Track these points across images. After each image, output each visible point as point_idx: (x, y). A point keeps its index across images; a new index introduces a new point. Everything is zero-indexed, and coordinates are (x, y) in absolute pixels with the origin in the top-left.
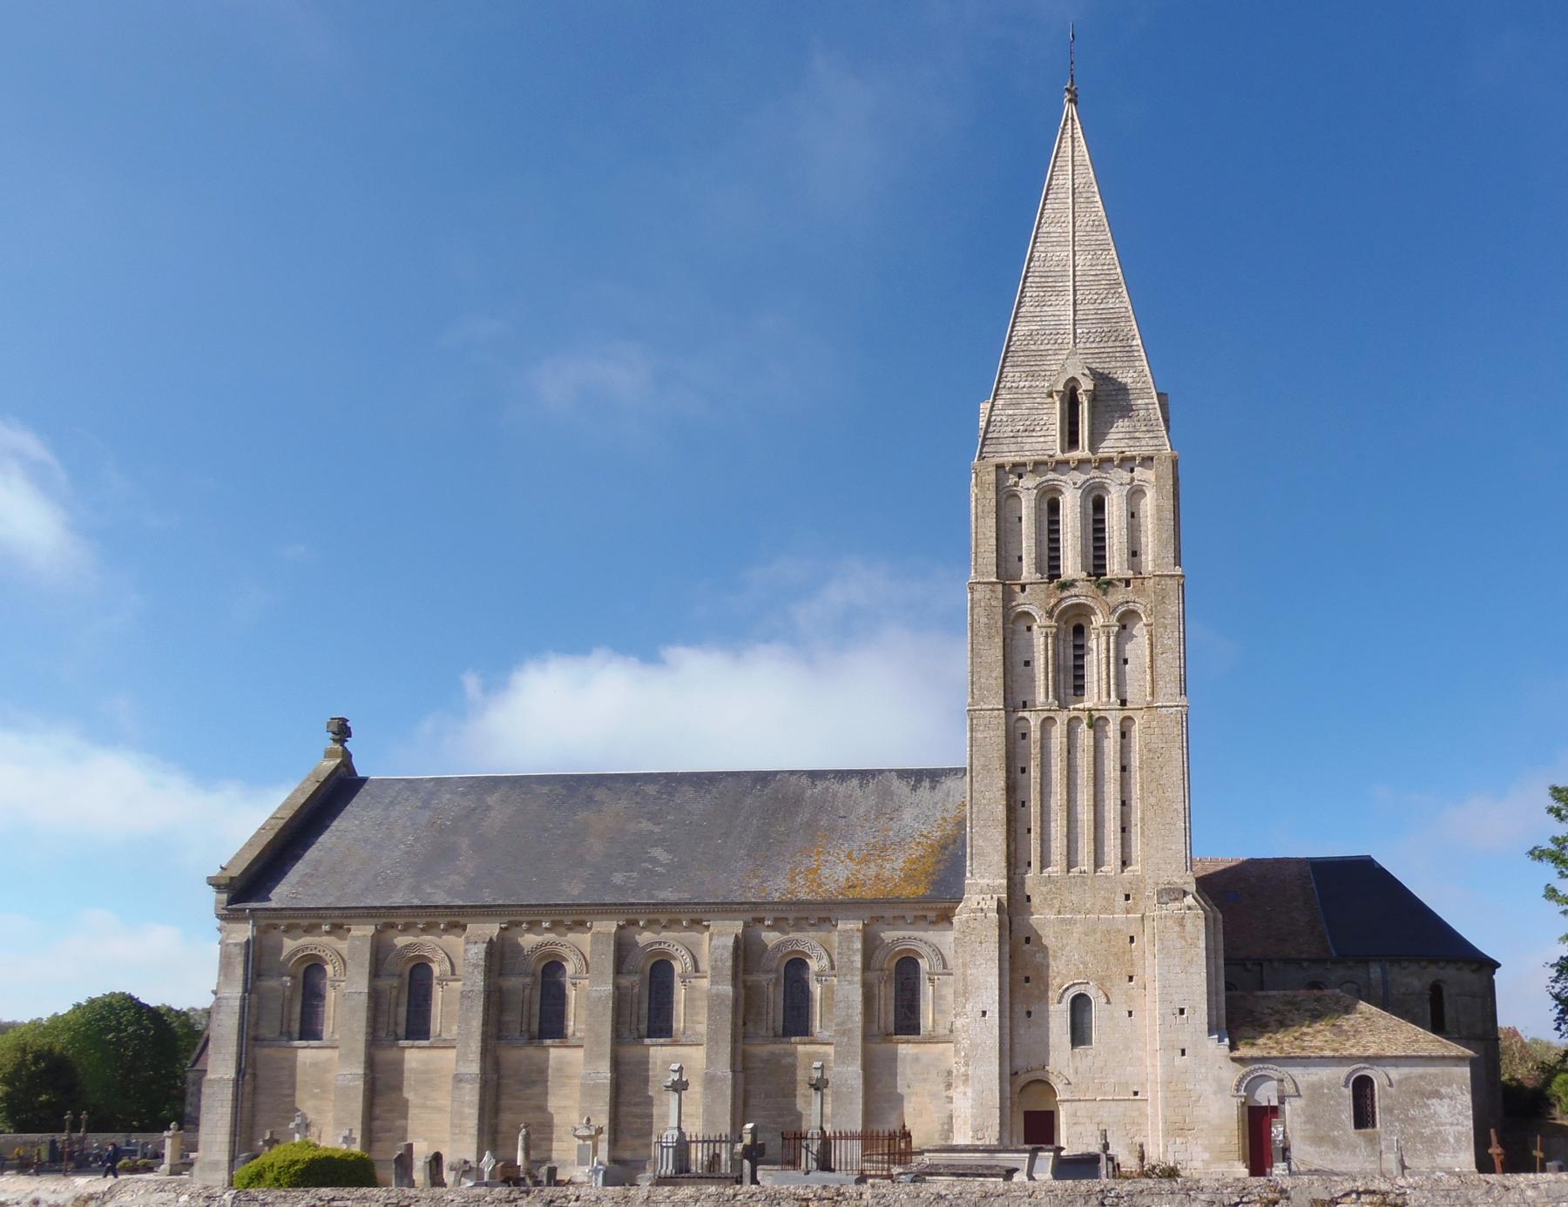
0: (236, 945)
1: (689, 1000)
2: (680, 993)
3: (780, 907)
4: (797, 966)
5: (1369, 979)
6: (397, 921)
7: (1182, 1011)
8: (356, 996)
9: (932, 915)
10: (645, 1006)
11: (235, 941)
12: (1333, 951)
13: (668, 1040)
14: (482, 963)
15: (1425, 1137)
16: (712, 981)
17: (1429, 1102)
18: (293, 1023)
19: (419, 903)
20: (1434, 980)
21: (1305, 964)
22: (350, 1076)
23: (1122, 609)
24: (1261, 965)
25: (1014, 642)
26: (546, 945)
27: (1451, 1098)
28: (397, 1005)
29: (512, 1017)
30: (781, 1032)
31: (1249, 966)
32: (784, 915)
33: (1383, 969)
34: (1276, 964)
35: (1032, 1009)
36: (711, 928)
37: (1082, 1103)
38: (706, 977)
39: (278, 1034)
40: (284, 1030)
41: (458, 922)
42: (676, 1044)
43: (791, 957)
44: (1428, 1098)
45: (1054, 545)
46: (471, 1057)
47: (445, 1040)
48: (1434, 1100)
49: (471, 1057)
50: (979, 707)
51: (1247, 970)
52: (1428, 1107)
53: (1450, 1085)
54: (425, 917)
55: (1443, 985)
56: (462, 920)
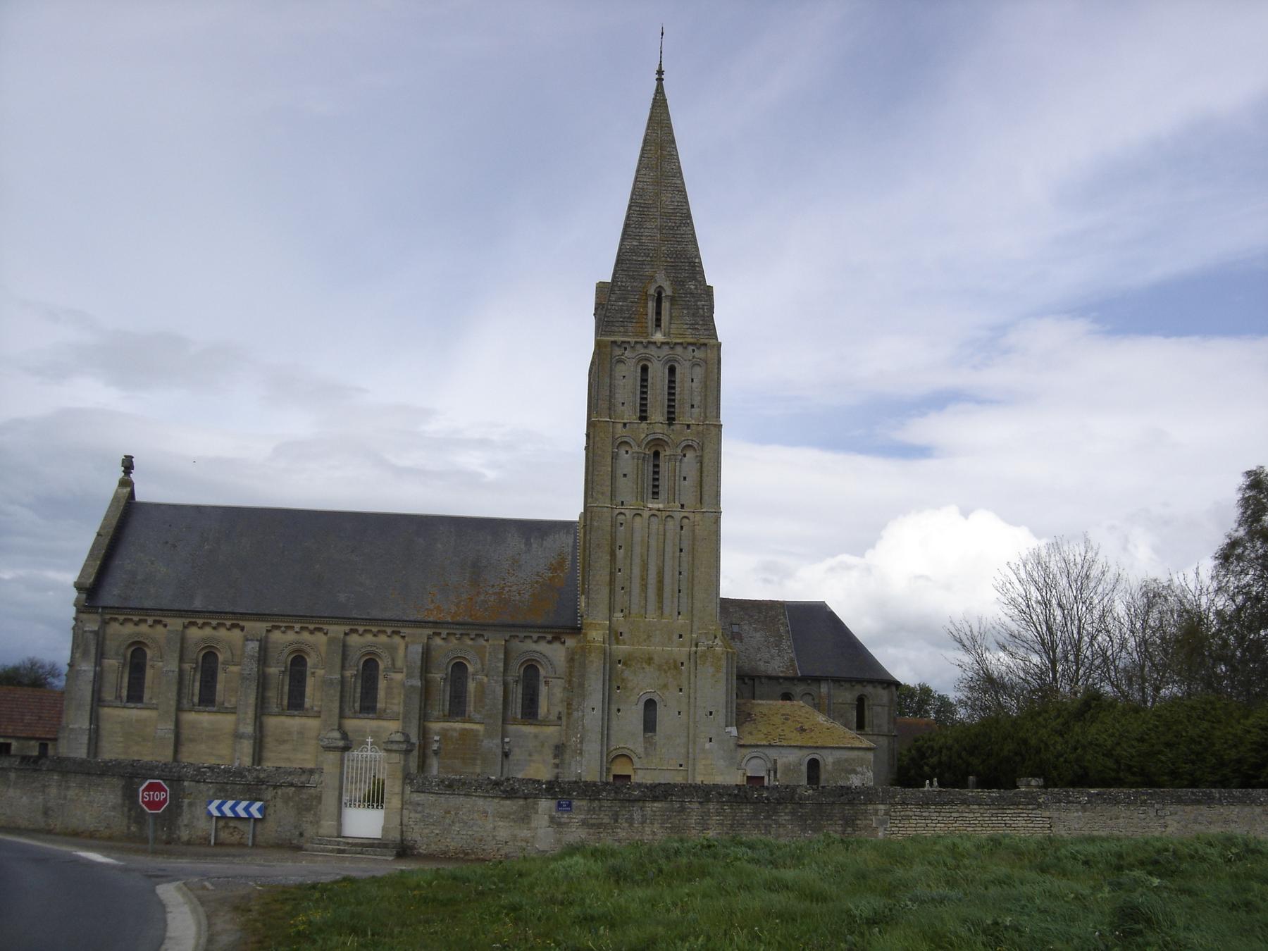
0: (91, 632)
1: (389, 689)
2: (382, 684)
3: (452, 626)
4: (459, 669)
5: (820, 692)
6: (281, 624)
7: (711, 713)
8: (171, 674)
9: (549, 637)
10: (359, 690)
11: (91, 629)
12: (799, 672)
13: (375, 716)
14: (256, 654)
15: (628, 823)
16: (407, 676)
17: (850, 776)
18: (123, 691)
19: (215, 609)
20: (859, 694)
21: (781, 681)
22: (166, 731)
23: (684, 444)
24: (754, 680)
25: (617, 461)
26: (303, 643)
27: (862, 775)
28: (194, 681)
29: (272, 694)
30: (358, 710)
31: (746, 680)
32: (481, 633)
33: (829, 689)
34: (763, 680)
35: (621, 708)
36: (406, 638)
37: (649, 771)
38: (402, 672)
39: (114, 697)
40: (118, 694)
41: (238, 624)
42: (379, 718)
43: (458, 660)
44: (849, 774)
45: (644, 402)
46: (248, 721)
47: (227, 708)
48: (852, 775)
49: (248, 721)
50: (596, 505)
51: (746, 684)
52: (849, 779)
53: (862, 766)
54: (217, 619)
55: (866, 699)
56: (242, 623)
